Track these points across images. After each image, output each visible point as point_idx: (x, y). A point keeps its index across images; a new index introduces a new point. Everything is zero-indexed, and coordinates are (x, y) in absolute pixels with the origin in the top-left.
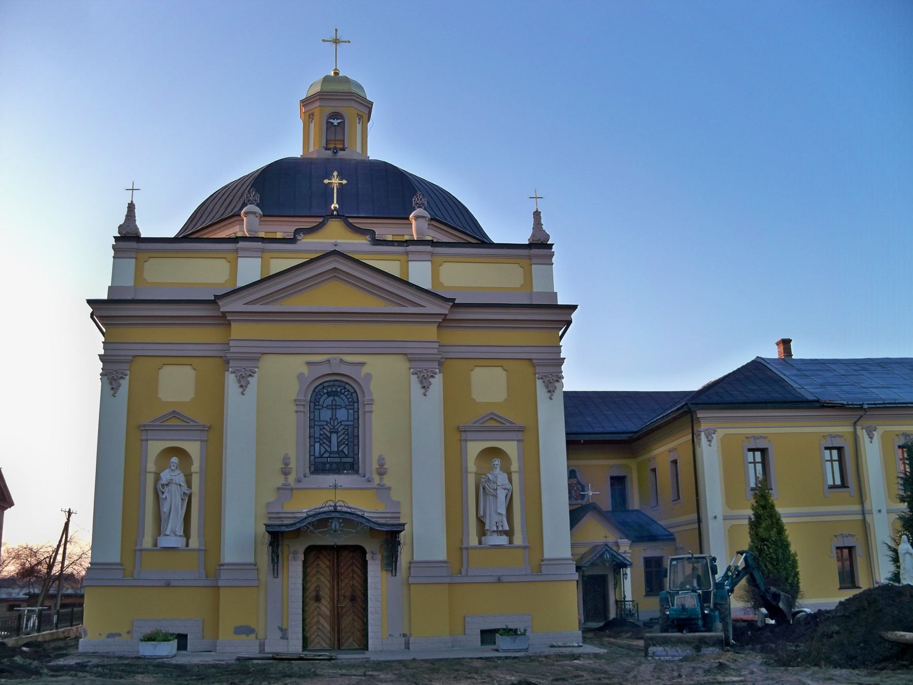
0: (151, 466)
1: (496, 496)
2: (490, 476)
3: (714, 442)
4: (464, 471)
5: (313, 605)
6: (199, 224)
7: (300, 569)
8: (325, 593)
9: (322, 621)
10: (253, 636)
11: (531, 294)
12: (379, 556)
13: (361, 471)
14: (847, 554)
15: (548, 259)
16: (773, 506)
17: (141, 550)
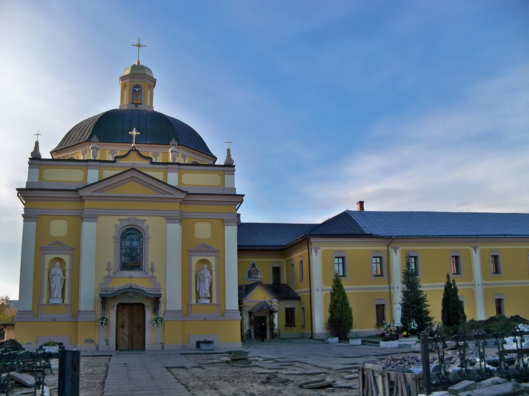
0: (47, 266)
1: (204, 282)
2: (202, 272)
3: (318, 254)
4: (190, 269)
5: (120, 330)
6: (68, 143)
7: (115, 313)
8: (126, 324)
9: (125, 337)
10: (93, 343)
11: (224, 188)
12: (151, 308)
13: (143, 269)
14: (380, 309)
15: (232, 173)
16: (342, 286)
17: (42, 305)
